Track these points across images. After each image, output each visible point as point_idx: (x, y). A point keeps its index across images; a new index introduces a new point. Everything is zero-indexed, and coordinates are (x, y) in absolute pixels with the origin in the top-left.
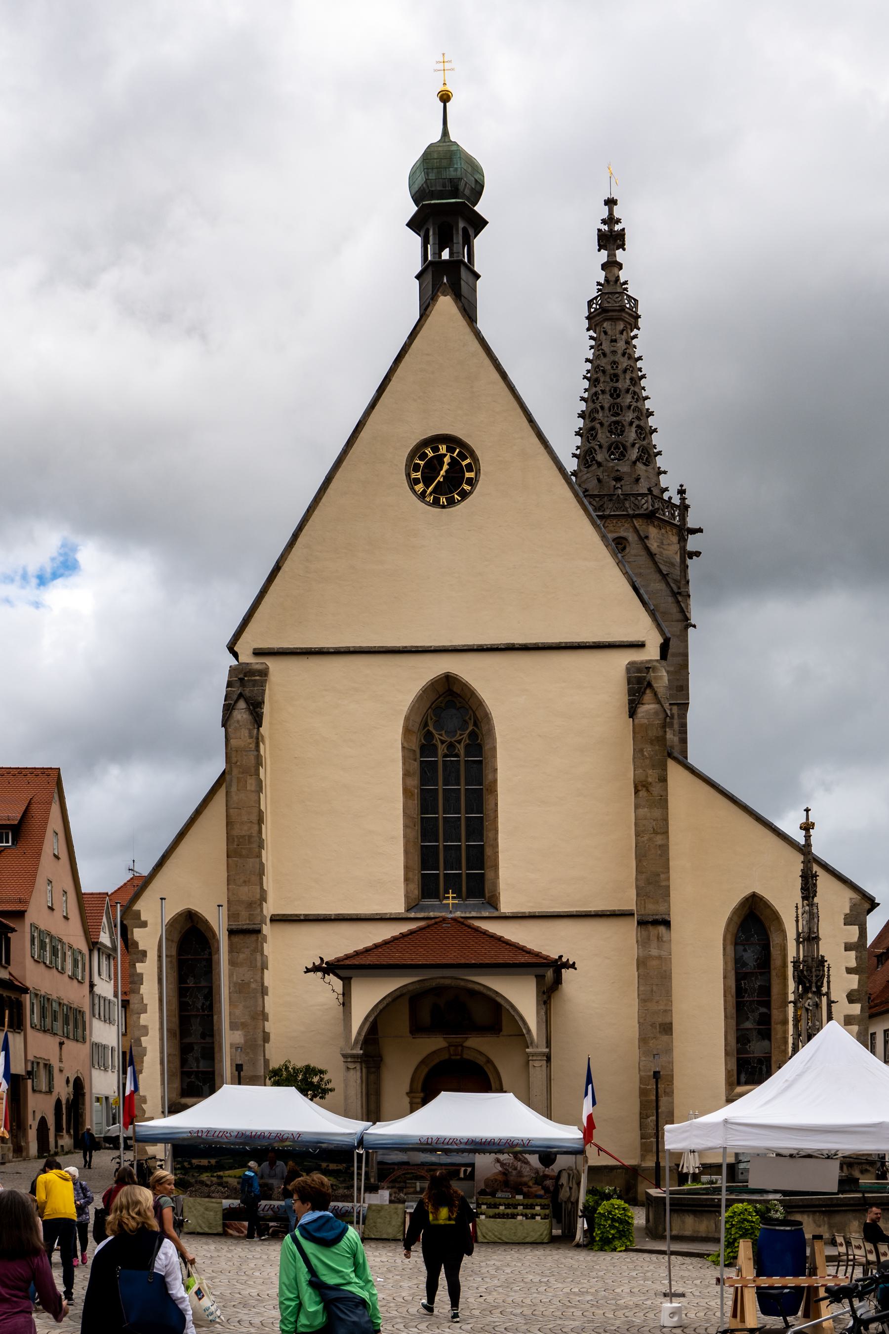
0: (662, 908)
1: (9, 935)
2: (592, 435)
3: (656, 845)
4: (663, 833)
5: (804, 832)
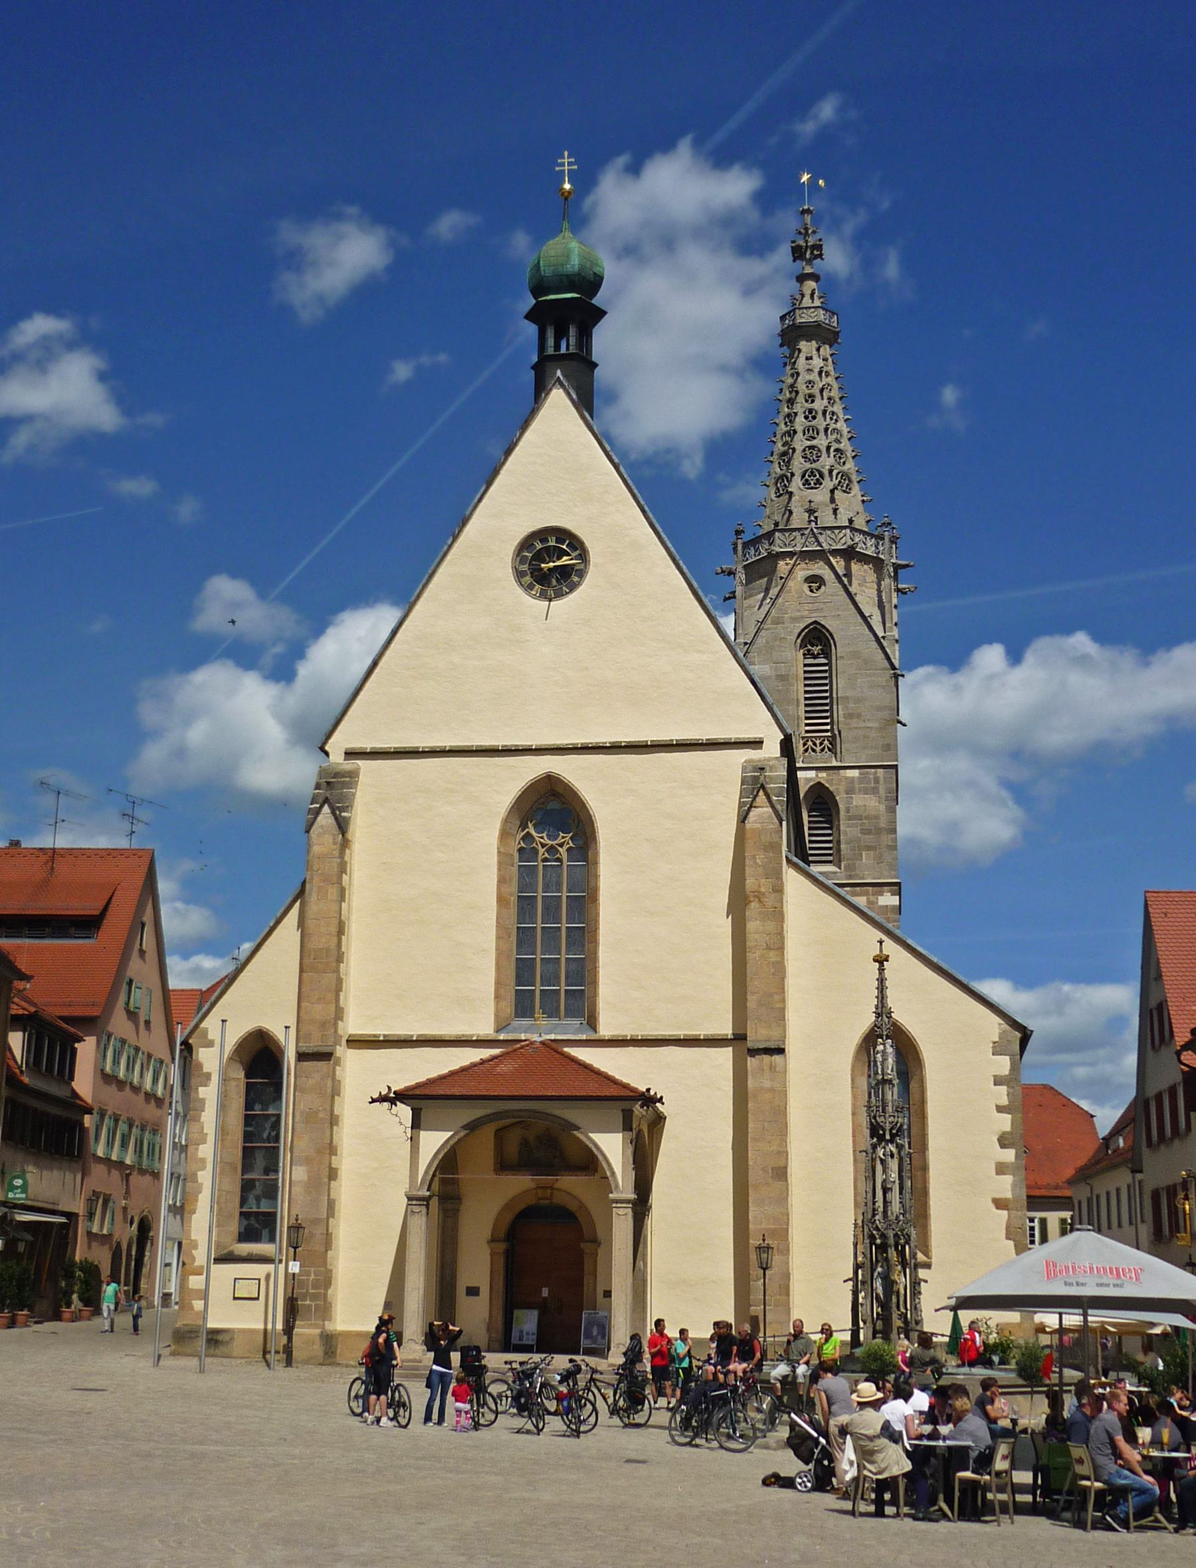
0: (775, 1033)
1: (76, 1045)
2: (784, 461)
3: (769, 962)
4: (778, 949)
5: (877, 964)
